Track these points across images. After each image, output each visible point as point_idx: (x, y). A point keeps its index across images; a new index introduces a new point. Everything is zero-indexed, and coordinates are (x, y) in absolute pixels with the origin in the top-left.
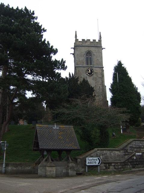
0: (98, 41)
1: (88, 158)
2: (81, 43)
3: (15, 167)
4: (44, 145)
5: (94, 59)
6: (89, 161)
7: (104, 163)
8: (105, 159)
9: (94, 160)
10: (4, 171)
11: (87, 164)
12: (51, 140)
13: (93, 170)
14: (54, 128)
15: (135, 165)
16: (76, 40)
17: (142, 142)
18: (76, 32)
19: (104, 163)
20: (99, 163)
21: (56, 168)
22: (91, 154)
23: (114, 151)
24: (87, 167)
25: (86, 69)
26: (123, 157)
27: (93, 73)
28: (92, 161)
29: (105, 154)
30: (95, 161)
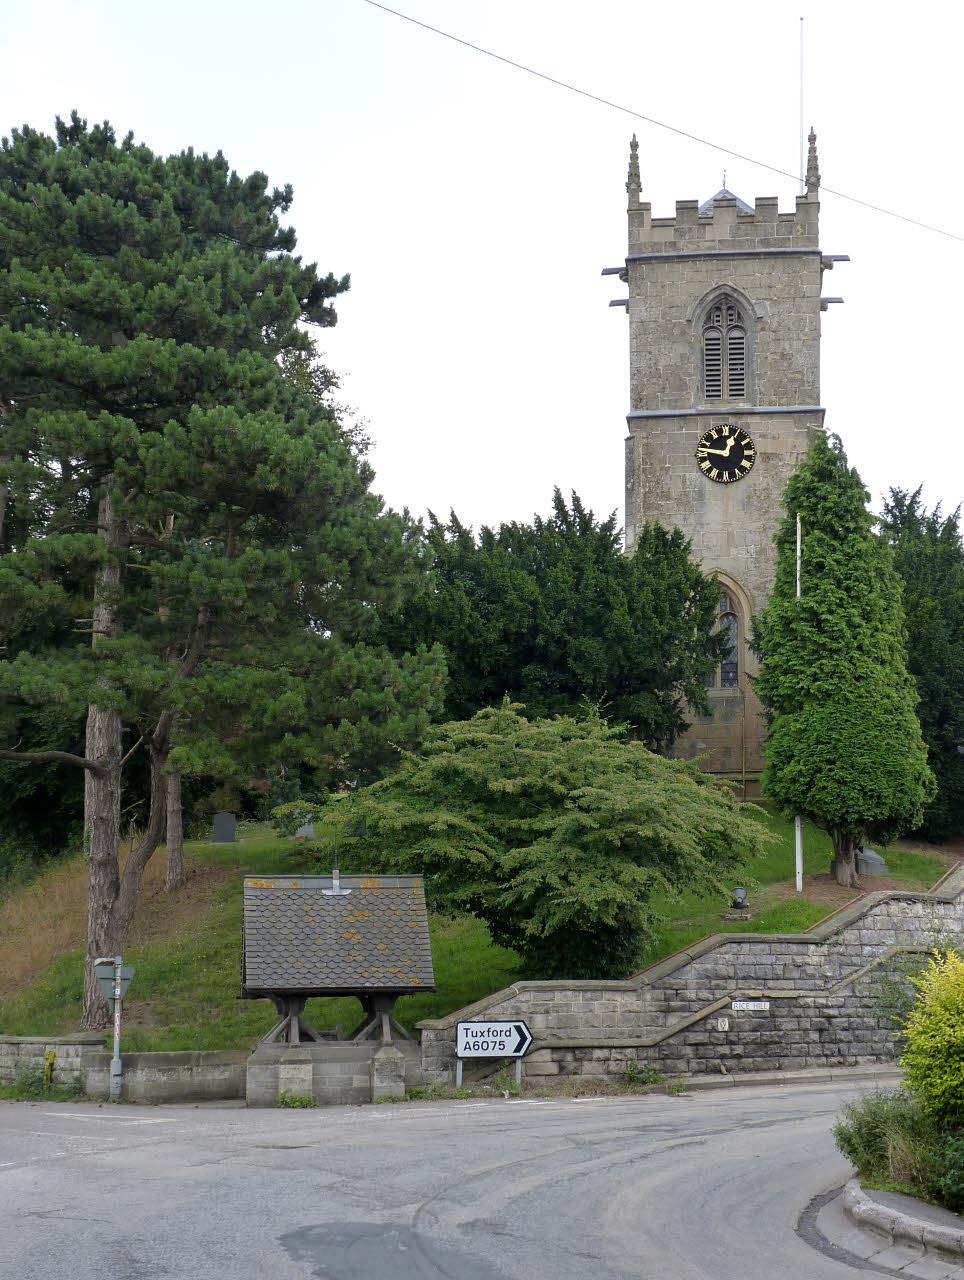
0: (794, 210)
1: (467, 1025)
2: (668, 235)
3: (163, 1071)
4: (268, 971)
5: (761, 350)
6: (471, 1040)
7: (554, 1049)
8: (555, 1031)
9: (496, 1033)
10: (117, 1091)
11: (461, 1052)
12: (302, 948)
13: (485, 1070)
14: (328, 893)
15: (723, 1057)
16: (638, 212)
17: (777, 947)
18: (634, 145)
19: (554, 1049)
20: (518, 1049)
21: (314, 1069)
22: (486, 1008)
23: (608, 995)
24: (460, 1065)
25: (700, 432)
26: (653, 1020)
27: (749, 458)
28: (486, 1039)
29: (557, 1008)
30: (498, 1039)
